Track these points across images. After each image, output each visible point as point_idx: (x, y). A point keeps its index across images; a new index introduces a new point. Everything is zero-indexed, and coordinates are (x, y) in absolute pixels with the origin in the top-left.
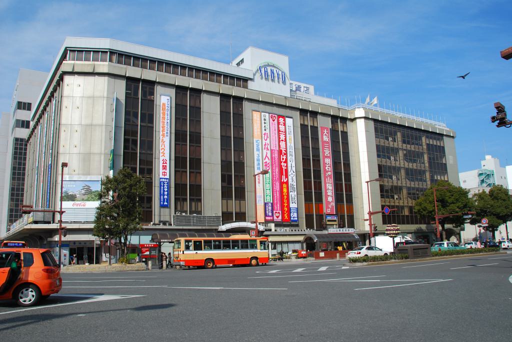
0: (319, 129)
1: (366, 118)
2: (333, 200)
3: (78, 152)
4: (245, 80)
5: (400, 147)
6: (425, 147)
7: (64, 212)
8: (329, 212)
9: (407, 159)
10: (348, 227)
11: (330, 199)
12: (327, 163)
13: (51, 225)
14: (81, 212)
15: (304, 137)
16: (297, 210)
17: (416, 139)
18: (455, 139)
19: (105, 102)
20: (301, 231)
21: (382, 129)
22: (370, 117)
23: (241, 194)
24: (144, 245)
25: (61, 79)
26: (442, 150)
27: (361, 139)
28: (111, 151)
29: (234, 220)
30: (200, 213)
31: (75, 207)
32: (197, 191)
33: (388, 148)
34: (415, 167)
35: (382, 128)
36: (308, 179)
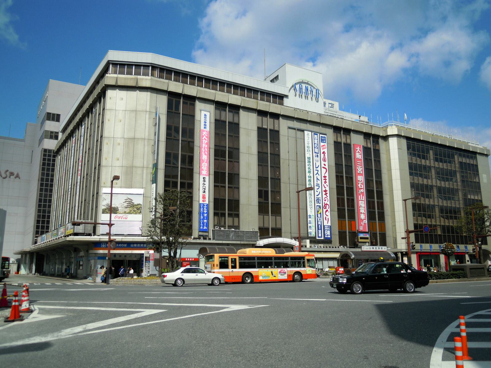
0: (352, 146)
2: (365, 217)
5: (432, 165)
6: (457, 165)
7: (114, 224)
8: (362, 229)
9: (439, 177)
10: (380, 245)
11: (362, 216)
12: (360, 180)
13: (92, 237)
14: (131, 226)
15: (338, 154)
16: (331, 229)
17: (449, 157)
18: (489, 157)
19: (147, 116)
20: (336, 247)
21: (414, 147)
22: (403, 135)
23: (277, 210)
24: (185, 259)
25: (102, 94)
26: (475, 169)
27: (394, 156)
28: (153, 165)
29: (270, 235)
30: (238, 227)
32: (235, 205)
33: (420, 166)
34: (447, 186)
35: (416, 146)
36: (341, 195)
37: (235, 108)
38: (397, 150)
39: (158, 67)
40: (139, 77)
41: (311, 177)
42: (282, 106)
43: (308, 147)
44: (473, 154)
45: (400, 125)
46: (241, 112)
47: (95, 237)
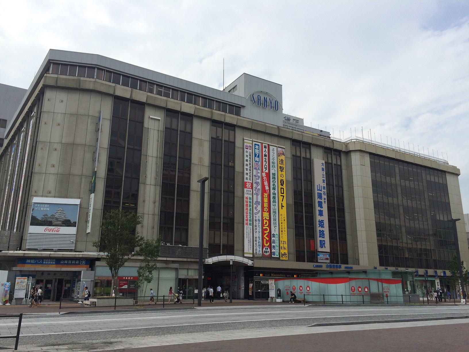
3: (56, 172)
6: (425, 184)
19: (89, 120)
25: (42, 93)
31: (47, 232)
32: (184, 219)
37: (189, 117)
39: (105, 70)
40: (82, 78)
41: (275, 194)
42: (239, 117)
43: (273, 163)
46: (238, 131)
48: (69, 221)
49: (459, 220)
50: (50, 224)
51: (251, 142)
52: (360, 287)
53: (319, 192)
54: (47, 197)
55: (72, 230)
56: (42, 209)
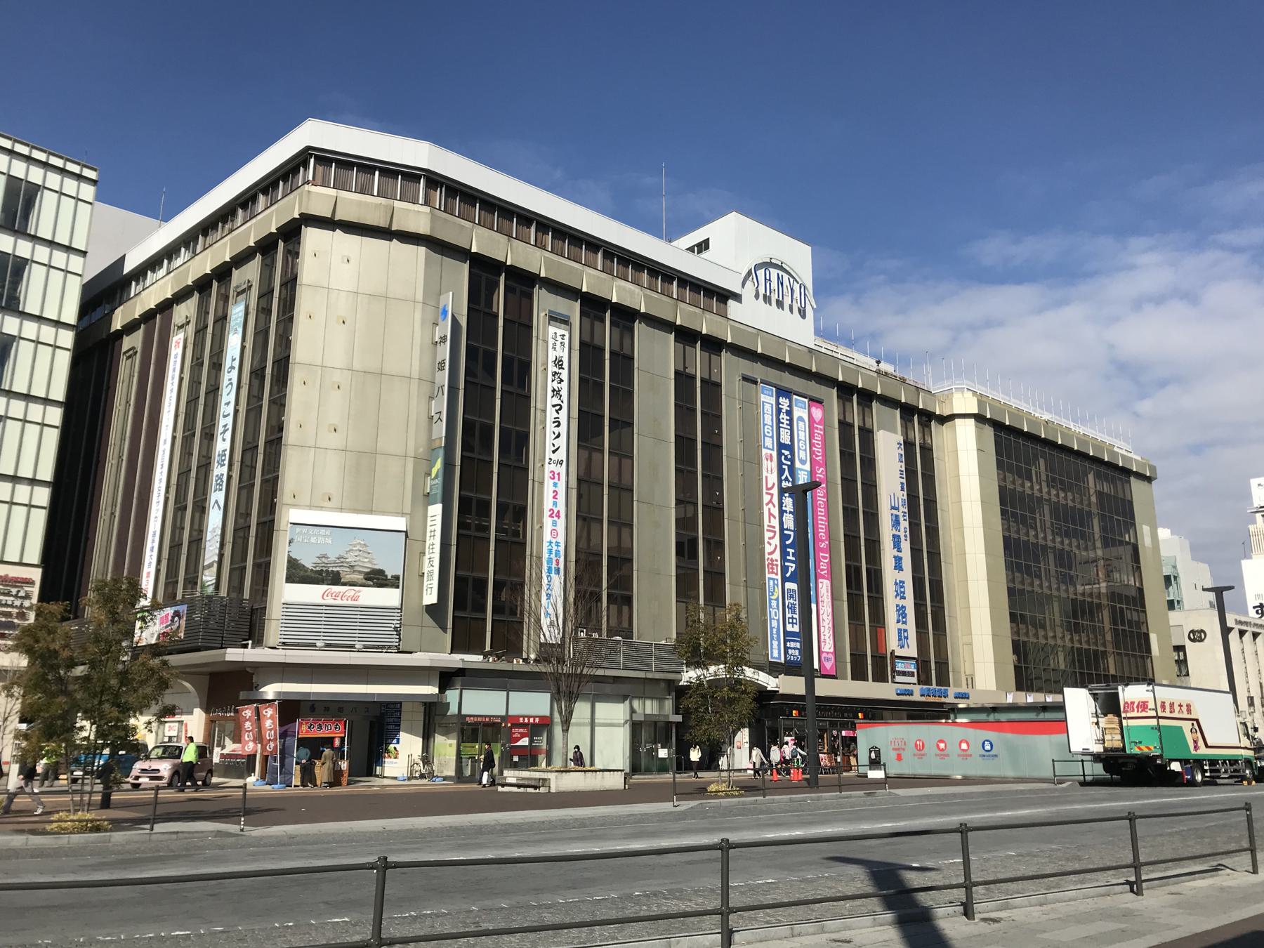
1: (979, 418)
4: (724, 296)
6: (1093, 499)
13: (249, 651)
19: (418, 315)
30: (628, 633)
31: (330, 601)
37: (626, 316)
38: (975, 452)
40: (344, 194)
44: (1118, 473)
45: (981, 390)
47: (258, 651)
48: (381, 572)
49: (1232, 588)
50: (335, 579)
51: (44, 352)
52: (941, 741)
53: (895, 512)
54: (321, 508)
55: (389, 597)
56: (313, 540)
